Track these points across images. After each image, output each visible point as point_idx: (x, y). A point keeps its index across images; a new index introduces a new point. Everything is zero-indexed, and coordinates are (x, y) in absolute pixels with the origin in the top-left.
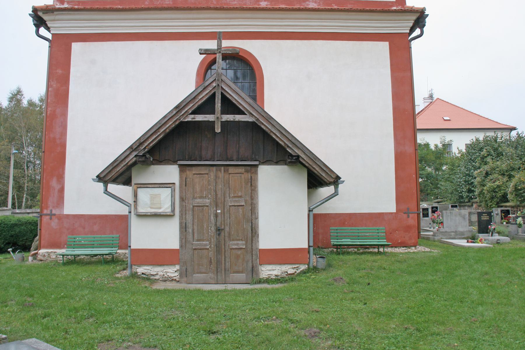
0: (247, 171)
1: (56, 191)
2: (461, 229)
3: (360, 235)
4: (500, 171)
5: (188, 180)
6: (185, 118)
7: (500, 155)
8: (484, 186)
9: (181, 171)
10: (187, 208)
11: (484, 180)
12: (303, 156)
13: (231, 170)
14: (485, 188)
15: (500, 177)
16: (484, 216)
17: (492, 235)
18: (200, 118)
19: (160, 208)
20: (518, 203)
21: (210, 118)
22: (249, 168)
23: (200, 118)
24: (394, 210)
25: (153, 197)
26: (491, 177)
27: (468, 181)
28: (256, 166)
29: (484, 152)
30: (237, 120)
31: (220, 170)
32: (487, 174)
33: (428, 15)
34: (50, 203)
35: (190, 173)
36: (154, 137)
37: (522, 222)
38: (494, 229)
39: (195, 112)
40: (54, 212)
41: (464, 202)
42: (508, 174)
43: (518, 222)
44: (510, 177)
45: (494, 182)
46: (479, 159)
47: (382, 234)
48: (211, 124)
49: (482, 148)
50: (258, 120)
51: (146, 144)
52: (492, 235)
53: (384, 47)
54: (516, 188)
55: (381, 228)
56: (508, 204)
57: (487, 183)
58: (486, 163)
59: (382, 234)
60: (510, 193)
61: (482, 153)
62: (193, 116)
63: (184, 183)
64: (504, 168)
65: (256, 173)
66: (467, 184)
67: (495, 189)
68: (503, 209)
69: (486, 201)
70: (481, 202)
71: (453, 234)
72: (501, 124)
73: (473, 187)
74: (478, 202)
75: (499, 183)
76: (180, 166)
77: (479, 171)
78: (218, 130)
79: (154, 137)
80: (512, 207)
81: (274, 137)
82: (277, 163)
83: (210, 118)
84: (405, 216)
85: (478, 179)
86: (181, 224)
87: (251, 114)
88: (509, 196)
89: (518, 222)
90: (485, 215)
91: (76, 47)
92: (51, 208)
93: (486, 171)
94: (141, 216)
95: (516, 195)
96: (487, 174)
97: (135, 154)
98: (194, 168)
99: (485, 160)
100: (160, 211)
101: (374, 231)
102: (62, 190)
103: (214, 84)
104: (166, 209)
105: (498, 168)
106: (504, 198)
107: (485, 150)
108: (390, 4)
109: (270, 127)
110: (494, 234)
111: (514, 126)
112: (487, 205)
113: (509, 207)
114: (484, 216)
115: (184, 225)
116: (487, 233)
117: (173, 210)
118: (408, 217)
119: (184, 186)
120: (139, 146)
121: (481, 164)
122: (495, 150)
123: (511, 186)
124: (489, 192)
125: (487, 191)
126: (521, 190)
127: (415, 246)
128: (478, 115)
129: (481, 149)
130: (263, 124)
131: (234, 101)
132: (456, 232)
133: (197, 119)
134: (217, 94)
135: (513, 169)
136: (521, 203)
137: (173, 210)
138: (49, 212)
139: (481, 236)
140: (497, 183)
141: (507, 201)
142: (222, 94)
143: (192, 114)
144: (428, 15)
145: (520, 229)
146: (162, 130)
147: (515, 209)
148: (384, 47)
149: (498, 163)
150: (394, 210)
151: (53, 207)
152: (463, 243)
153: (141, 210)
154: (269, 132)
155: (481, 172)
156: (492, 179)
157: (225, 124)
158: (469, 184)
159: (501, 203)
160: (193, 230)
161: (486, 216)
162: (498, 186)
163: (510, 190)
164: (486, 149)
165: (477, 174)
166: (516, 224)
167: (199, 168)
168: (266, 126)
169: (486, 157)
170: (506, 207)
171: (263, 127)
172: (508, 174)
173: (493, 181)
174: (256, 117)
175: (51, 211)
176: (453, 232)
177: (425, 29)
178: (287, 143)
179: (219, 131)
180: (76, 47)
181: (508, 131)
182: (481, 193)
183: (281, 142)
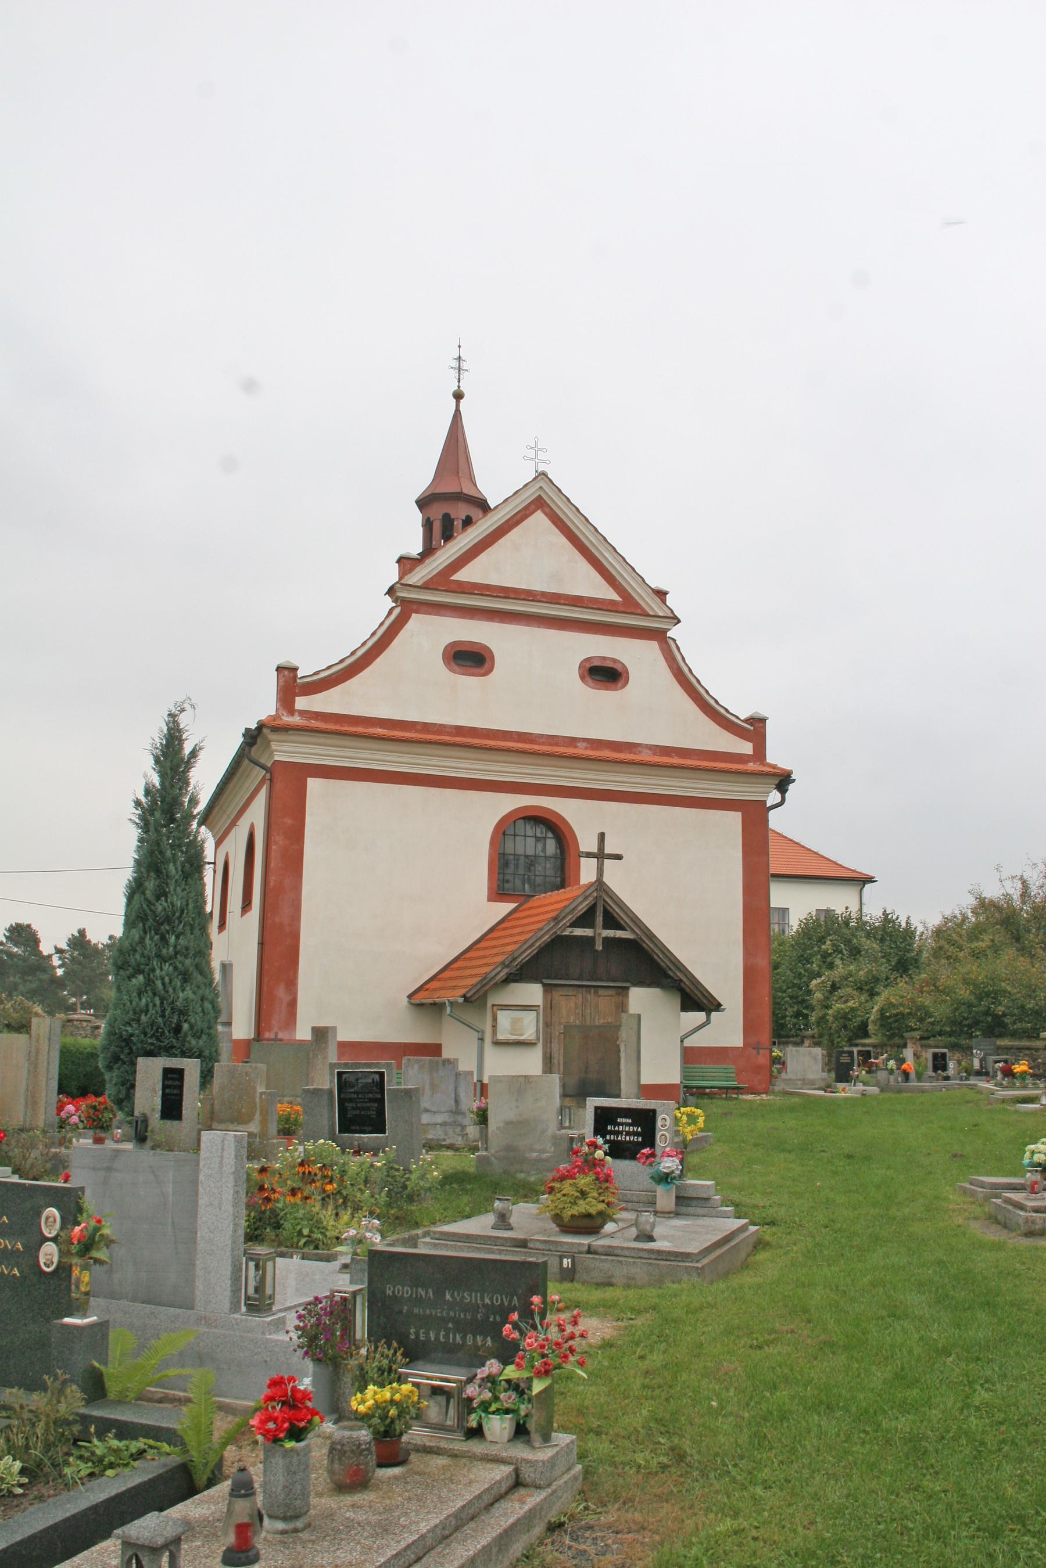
0: (618, 994)
1: (284, 1003)
2: (810, 1076)
3: (705, 1074)
4: (855, 983)
5: (554, 1002)
6: (562, 932)
7: (855, 952)
8: (827, 1007)
9: (545, 992)
10: (553, 1035)
11: (828, 998)
12: (685, 980)
13: (601, 992)
14: (830, 1012)
15: (855, 992)
16: (622, 1124)
17: (854, 1085)
18: (578, 932)
19: (522, 1035)
20: (885, 1039)
21: (588, 932)
22: (620, 990)
23: (578, 932)
24: (740, 1044)
25: (515, 1022)
26: (840, 992)
27: (797, 997)
28: (627, 988)
29: (827, 946)
30: (617, 936)
31: (590, 992)
32: (834, 987)
33: (794, 780)
34: (274, 1022)
35: (557, 994)
36: (529, 952)
37: (894, 1067)
38: (858, 1076)
39: (574, 925)
40: (280, 1035)
41: (788, 1036)
42: (869, 988)
43: (889, 1067)
44: (872, 994)
45: (846, 1002)
46: (819, 957)
47: (732, 1075)
48: (591, 940)
49: (824, 937)
50: (641, 938)
51: (519, 960)
52: (854, 1085)
53: (734, 819)
54: (882, 1014)
55: (730, 1066)
56: (867, 1041)
57: (834, 1002)
58: (831, 966)
59: (732, 1075)
60: (873, 1021)
61: (823, 947)
62: (570, 929)
63: (550, 1007)
64: (862, 978)
65: (627, 996)
66: (794, 1003)
67: (847, 1014)
68: (860, 1048)
69: (830, 1035)
70: (821, 1036)
71: (799, 1082)
72: (844, 867)
73: (807, 1008)
74: (816, 1036)
75: (854, 1003)
76: (544, 985)
77: (819, 980)
78: (599, 947)
79: (529, 952)
80: (874, 1046)
81: (656, 957)
82: (649, 985)
83: (588, 932)
84: (754, 1052)
85: (818, 995)
86: (544, 1054)
87: (633, 930)
88: (871, 1027)
89: (889, 1067)
90: (624, 1120)
91: (314, 786)
92: (276, 1029)
93: (833, 982)
94: (497, 1043)
95: (881, 1026)
96: (834, 987)
97: (506, 971)
98: (559, 989)
99: (829, 960)
100: (522, 1038)
101: (721, 1070)
102: (293, 1004)
103: (595, 894)
104: (531, 1035)
105: (851, 976)
106: (863, 1031)
107: (828, 942)
108: (746, 758)
109: (652, 946)
110: (857, 1084)
111: (871, 874)
112: (832, 1042)
113: (868, 1045)
114: (622, 1124)
115: (548, 1055)
116: (847, 1081)
117: (538, 1039)
118: (758, 1053)
119: (549, 1010)
120: (511, 962)
121: (820, 967)
122: (848, 942)
123: (874, 1010)
124: (836, 1019)
125: (834, 1017)
126: (889, 1017)
127: (766, 1093)
128: (797, 843)
129: (822, 940)
130: (645, 942)
131: (615, 915)
132: (803, 1080)
133: (575, 934)
134: (598, 905)
135: (877, 980)
136: (888, 1040)
137: (538, 1039)
138: (272, 1036)
139: (840, 1085)
140: (850, 1004)
141: (866, 1035)
142: (604, 907)
143: (570, 926)
144: (794, 780)
145: (892, 1078)
146: (537, 945)
147: (879, 1050)
148: (734, 819)
149: (852, 967)
150: (740, 1044)
151: (280, 1029)
152: (822, 1093)
153: (501, 1037)
154: (650, 952)
155: (823, 982)
156: (842, 997)
157: (606, 940)
158: (798, 1003)
159: (856, 1039)
160: (559, 1061)
161: (629, 1125)
162: (852, 1009)
163: (872, 1017)
164: (831, 941)
165: (816, 986)
166: (887, 1069)
167: (566, 989)
168: (648, 944)
169: (830, 955)
170: (864, 1045)
171: (644, 945)
172: (869, 988)
173: (843, 999)
174: (637, 934)
175: (276, 1034)
176: (800, 1080)
177: (787, 795)
178: (669, 965)
179: (601, 948)
180: (314, 786)
181: (859, 885)
182: (822, 1020)
183: (662, 964)
